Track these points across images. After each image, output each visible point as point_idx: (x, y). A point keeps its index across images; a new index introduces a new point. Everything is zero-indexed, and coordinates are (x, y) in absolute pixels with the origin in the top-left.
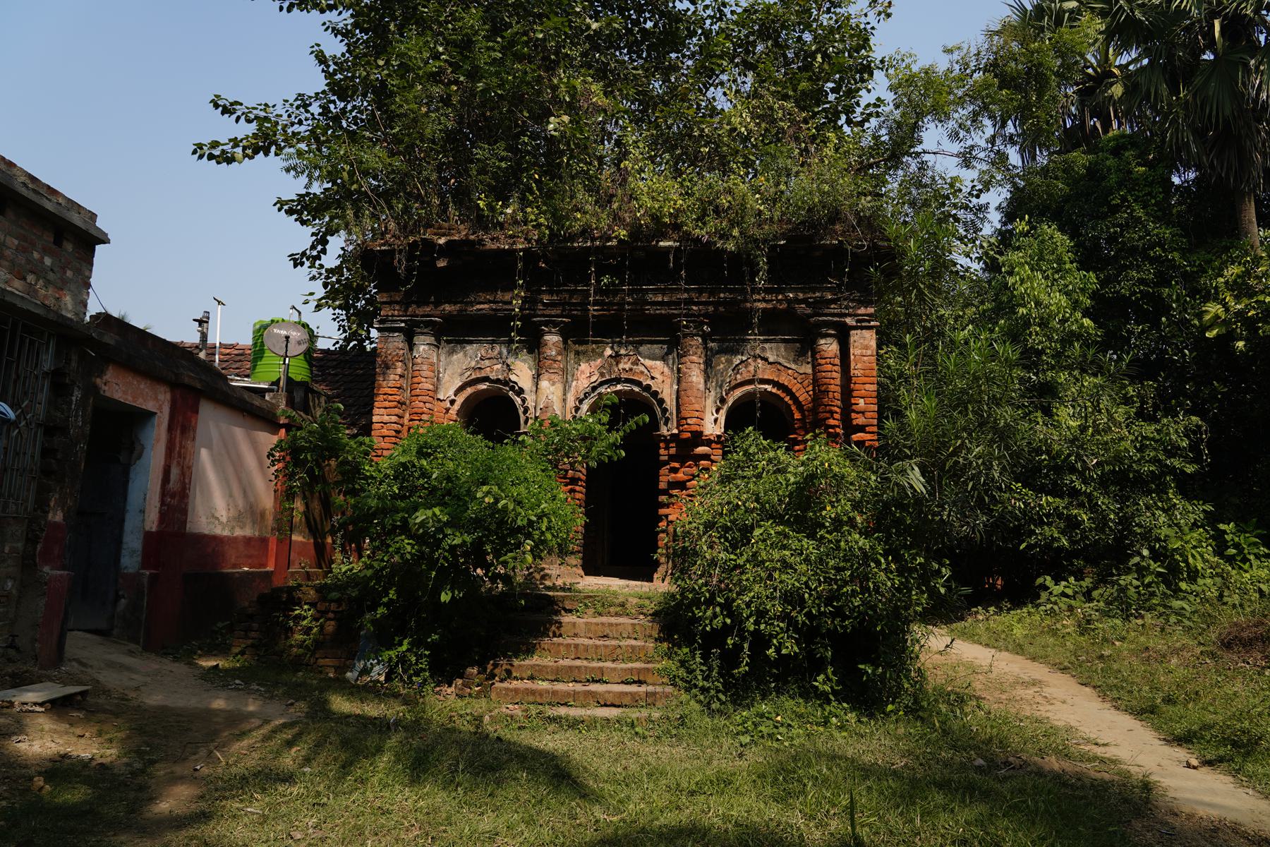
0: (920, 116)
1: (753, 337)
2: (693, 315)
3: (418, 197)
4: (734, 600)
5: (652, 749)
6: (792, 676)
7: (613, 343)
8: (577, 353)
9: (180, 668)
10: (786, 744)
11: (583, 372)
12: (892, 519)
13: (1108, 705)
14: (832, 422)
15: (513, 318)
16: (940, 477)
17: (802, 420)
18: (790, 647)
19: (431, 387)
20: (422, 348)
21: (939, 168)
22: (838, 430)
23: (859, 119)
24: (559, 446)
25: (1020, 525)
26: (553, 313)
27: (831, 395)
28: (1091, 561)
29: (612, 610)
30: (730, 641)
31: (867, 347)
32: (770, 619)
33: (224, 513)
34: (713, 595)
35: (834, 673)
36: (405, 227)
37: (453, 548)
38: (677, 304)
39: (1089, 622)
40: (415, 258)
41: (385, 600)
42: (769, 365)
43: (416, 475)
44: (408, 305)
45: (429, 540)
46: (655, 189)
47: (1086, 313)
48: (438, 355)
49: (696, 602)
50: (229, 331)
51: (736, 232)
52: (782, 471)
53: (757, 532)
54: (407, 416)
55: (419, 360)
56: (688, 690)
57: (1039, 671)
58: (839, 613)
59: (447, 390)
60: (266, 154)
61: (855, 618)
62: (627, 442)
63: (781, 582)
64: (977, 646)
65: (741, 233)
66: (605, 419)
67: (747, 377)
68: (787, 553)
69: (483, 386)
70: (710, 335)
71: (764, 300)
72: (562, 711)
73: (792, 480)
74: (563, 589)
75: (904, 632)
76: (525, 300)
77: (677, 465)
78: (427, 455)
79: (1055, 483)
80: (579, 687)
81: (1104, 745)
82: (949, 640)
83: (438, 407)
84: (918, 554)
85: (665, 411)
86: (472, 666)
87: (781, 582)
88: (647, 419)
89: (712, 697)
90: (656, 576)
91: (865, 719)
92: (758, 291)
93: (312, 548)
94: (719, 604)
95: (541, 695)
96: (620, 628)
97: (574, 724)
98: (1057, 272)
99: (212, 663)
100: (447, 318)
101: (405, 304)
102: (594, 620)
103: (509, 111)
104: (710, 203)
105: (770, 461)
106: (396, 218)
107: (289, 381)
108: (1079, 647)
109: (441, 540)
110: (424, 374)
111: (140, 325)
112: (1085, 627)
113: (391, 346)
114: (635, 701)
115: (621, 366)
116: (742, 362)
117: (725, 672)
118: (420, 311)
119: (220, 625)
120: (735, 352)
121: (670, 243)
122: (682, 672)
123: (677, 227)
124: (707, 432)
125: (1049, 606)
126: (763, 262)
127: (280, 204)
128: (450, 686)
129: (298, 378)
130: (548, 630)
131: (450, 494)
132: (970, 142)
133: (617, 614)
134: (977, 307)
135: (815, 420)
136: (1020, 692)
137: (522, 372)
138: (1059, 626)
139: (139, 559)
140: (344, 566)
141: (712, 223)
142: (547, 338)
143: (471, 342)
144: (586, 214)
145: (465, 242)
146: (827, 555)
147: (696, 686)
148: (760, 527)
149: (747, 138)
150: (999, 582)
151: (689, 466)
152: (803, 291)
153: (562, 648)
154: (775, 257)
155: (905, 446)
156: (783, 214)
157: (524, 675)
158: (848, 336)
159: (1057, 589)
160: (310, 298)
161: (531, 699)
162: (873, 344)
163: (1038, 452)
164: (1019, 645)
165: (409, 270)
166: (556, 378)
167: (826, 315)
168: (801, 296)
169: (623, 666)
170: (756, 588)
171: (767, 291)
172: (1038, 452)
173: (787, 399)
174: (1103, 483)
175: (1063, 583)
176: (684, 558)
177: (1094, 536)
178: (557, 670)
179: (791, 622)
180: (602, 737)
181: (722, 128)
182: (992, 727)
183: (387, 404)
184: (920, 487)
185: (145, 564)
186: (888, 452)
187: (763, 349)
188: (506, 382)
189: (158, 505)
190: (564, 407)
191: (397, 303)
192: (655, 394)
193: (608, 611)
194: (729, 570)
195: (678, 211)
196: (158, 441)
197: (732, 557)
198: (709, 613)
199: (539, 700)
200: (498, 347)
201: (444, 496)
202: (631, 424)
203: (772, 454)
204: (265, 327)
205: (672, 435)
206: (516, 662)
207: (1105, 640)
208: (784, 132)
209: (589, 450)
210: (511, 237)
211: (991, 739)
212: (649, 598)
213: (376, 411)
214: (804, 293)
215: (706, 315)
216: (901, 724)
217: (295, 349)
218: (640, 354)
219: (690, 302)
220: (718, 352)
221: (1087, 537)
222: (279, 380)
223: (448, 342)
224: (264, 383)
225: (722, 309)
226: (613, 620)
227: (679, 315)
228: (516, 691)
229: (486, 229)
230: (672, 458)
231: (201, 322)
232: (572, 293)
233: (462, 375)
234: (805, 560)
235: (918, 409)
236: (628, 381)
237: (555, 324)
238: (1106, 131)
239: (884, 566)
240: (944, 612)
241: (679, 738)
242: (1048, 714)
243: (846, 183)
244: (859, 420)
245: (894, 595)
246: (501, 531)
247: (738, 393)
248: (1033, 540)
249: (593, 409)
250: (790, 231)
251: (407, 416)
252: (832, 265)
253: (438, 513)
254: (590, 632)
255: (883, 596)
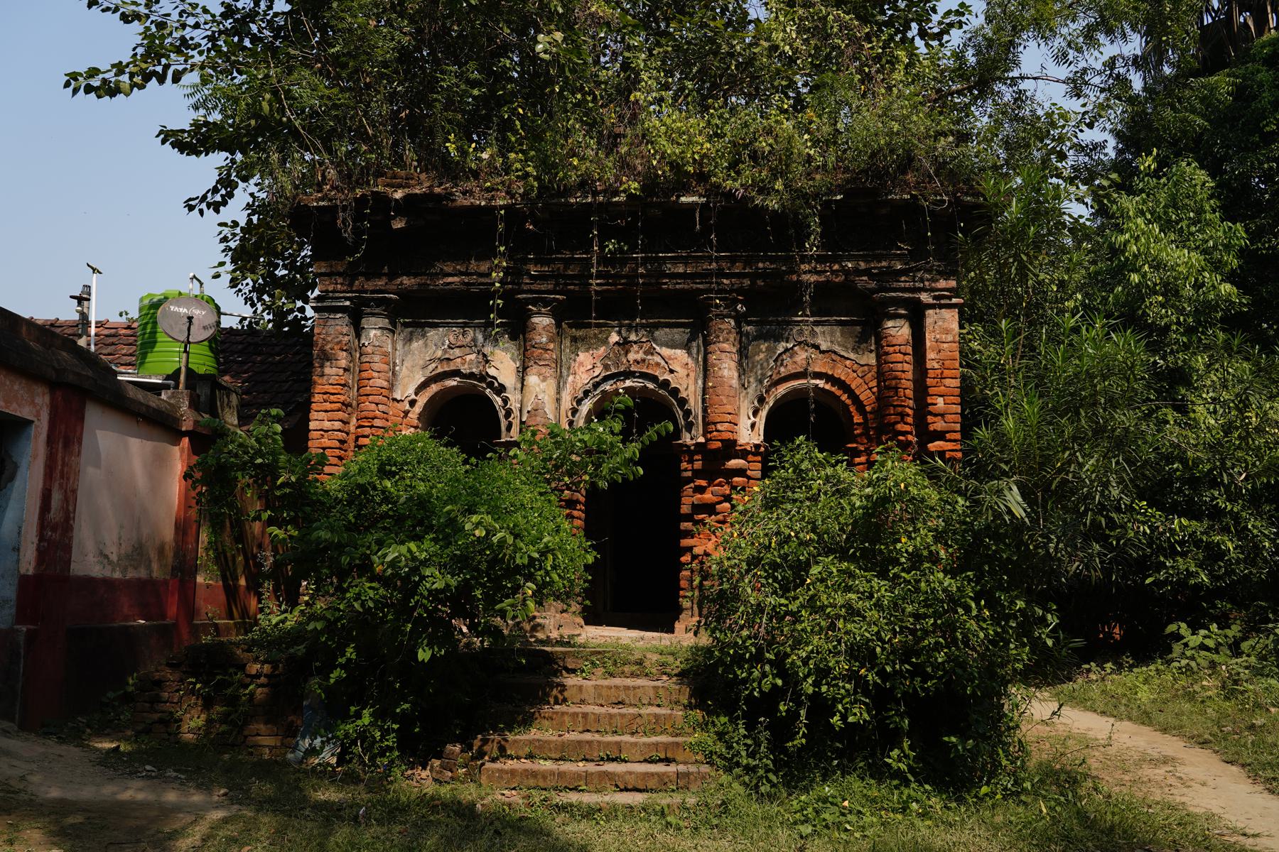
0: (1016, 31)
1: (803, 318)
2: (724, 291)
3: (365, 138)
4: (788, 656)
5: (689, 843)
6: (860, 750)
7: (621, 326)
8: (574, 340)
9: (71, 751)
10: (857, 835)
11: (581, 364)
12: (987, 554)
13: (1261, 788)
14: (900, 427)
15: (492, 295)
16: (1045, 501)
17: (865, 425)
18: (859, 715)
19: (385, 384)
20: (372, 333)
21: (1039, 97)
22: (910, 437)
23: (936, 30)
24: (558, 461)
25: (1145, 556)
26: (543, 287)
27: (901, 392)
28: (1239, 604)
29: (627, 669)
30: (782, 708)
31: (947, 332)
32: (835, 678)
33: (114, 549)
34: (760, 651)
35: (911, 748)
36: (349, 176)
37: (434, 594)
38: (706, 275)
39: (1236, 682)
40: (364, 217)
41: (342, 660)
42: (821, 354)
43: (378, 499)
44: (353, 277)
45: (404, 582)
46: (674, 129)
47: (1231, 278)
48: (394, 343)
49: (739, 660)
50: (113, 306)
51: (779, 185)
52: (843, 493)
53: (815, 570)
54: (354, 421)
55: (369, 349)
56: (728, 770)
57: (1171, 745)
58: (918, 671)
59: (405, 387)
60: (162, 79)
61: (940, 678)
62: (646, 457)
63: (847, 633)
64: (1090, 715)
65: (786, 186)
66: (617, 427)
67: (792, 369)
68: (854, 596)
69: (452, 383)
70: (745, 315)
71: (814, 271)
72: (573, 797)
73: (858, 504)
74: (560, 643)
75: (999, 696)
76: (507, 271)
77: (703, 483)
78: (391, 475)
79: (1190, 501)
80: (591, 767)
81: (1254, 836)
82: (1055, 706)
83: (394, 409)
84: (1017, 597)
85: (687, 413)
86: (453, 742)
87: (847, 633)
88: (671, 428)
89: (761, 777)
90: (677, 625)
91: (954, 805)
92: (804, 259)
93: (221, 590)
94: (770, 662)
95: (544, 778)
96: (639, 693)
97: (590, 813)
98: (1194, 224)
99: (108, 745)
100: (404, 294)
101: (350, 275)
102: (606, 683)
103: (484, 24)
104: (745, 146)
105: (827, 479)
106: (338, 165)
107: (190, 372)
108: (1223, 715)
109: (417, 584)
110: (376, 366)
111: (27, 316)
112: (1231, 689)
113: (331, 330)
114: (663, 784)
115: (632, 356)
116: (787, 350)
117: (777, 745)
118: (369, 285)
119: (111, 695)
120: (778, 338)
121: (695, 199)
122: (720, 748)
123: (702, 177)
124: (741, 441)
125: (1184, 662)
126: (815, 224)
127: (169, 136)
128: (424, 768)
129: (201, 370)
130: (548, 695)
131: (417, 518)
132: (1082, 64)
133: (633, 675)
134: (1087, 269)
135: (881, 427)
136: (1147, 772)
137: (503, 365)
138: (1197, 688)
139: (13, 611)
140: (275, 617)
141: (748, 173)
142: (536, 320)
143: (435, 326)
144: (584, 158)
145: (429, 196)
146: (904, 599)
147: (738, 764)
148: (817, 563)
149: (792, 60)
150: (1117, 630)
151: (720, 485)
152: (865, 259)
153: (566, 718)
154: (830, 215)
155: (1001, 460)
156: (839, 159)
157: (521, 753)
158: (923, 316)
159: (1194, 640)
160: (220, 269)
161: (532, 782)
162: (955, 326)
163: (1169, 459)
164: (1145, 712)
165: (357, 232)
166: (548, 371)
167: (895, 290)
168: (863, 265)
169: (645, 739)
170: (815, 640)
171: (820, 259)
172: (1169, 459)
173: (844, 397)
174: (1255, 500)
175: (1203, 632)
176: (719, 605)
177: (1242, 570)
178: (563, 746)
179: (860, 683)
180: (626, 828)
181: (757, 45)
182: (1113, 814)
183: (328, 406)
184: (1019, 512)
185: (21, 617)
186: (981, 468)
187: (813, 334)
188: (483, 377)
189: (36, 540)
190: (558, 409)
191: (340, 274)
192: (675, 392)
193: (622, 672)
194: (777, 615)
195: (704, 156)
196: (35, 457)
197: (783, 601)
198: (756, 674)
199: (542, 784)
200: (471, 332)
201: (414, 527)
202: (651, 434)
203: (829, 471)
204: (155, 305)
205: (697, 444)
206: (510, 737)
207: (1257, 706)
208: (841, 53)
209: (598, 466)
210: (488, 190)
211: (1112, 828)
212: (673, 654)
213: (313, 415)
214: (866, 261)
215: (740, 291)
216: (999, 810)
217: (199, 334)
218: (655, 340)
219: (721, 274)
220: (756, 338)
221: (1233, 571)
222: (179, 370)
223: (406, 325)
224: (156, 376)
225: (760, 283)
226: (629, 682)
227: (709, 291)
228: (513, 772)
229: (455, 179)
230: (697, 474)
231: (80, 300)
232: (568, 262)
233: (424, 367)
234: (875, 605)
235: (1017, 417)
236: (644, 376)
237: (546, 303)
238: (1260, 32)
239: (974, 613)
240: (1048, 670)
241: (722, 830)
242: (1184, 799)
243: (920, 122)
244: (938, 425)
245: (987, 649)
246: (494, 574)
247: (782, 390)
248: (1162, 575)
249: (600, 412)
250: (848, 181)
251: (354, 421)
252: (904, 224)
253: (414, 548)
254: (601, 697)
255: (974, 649)
